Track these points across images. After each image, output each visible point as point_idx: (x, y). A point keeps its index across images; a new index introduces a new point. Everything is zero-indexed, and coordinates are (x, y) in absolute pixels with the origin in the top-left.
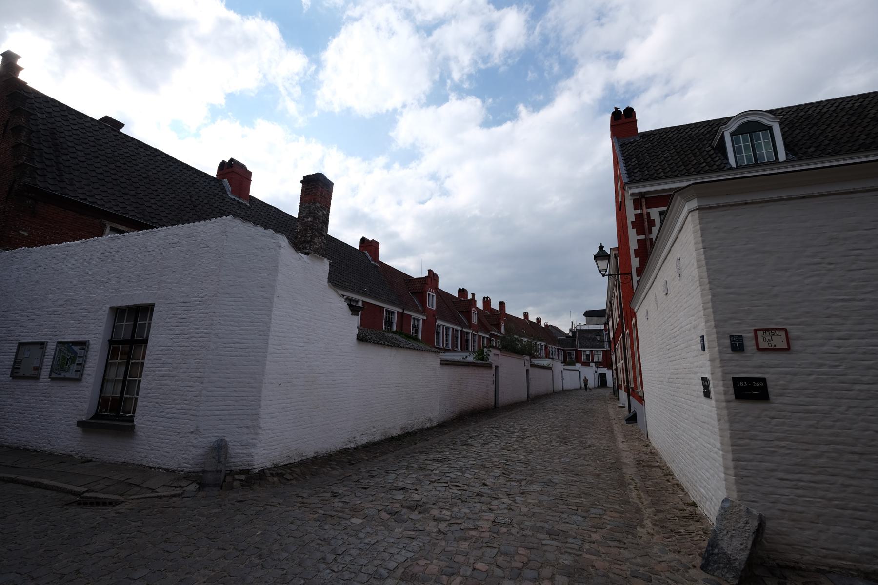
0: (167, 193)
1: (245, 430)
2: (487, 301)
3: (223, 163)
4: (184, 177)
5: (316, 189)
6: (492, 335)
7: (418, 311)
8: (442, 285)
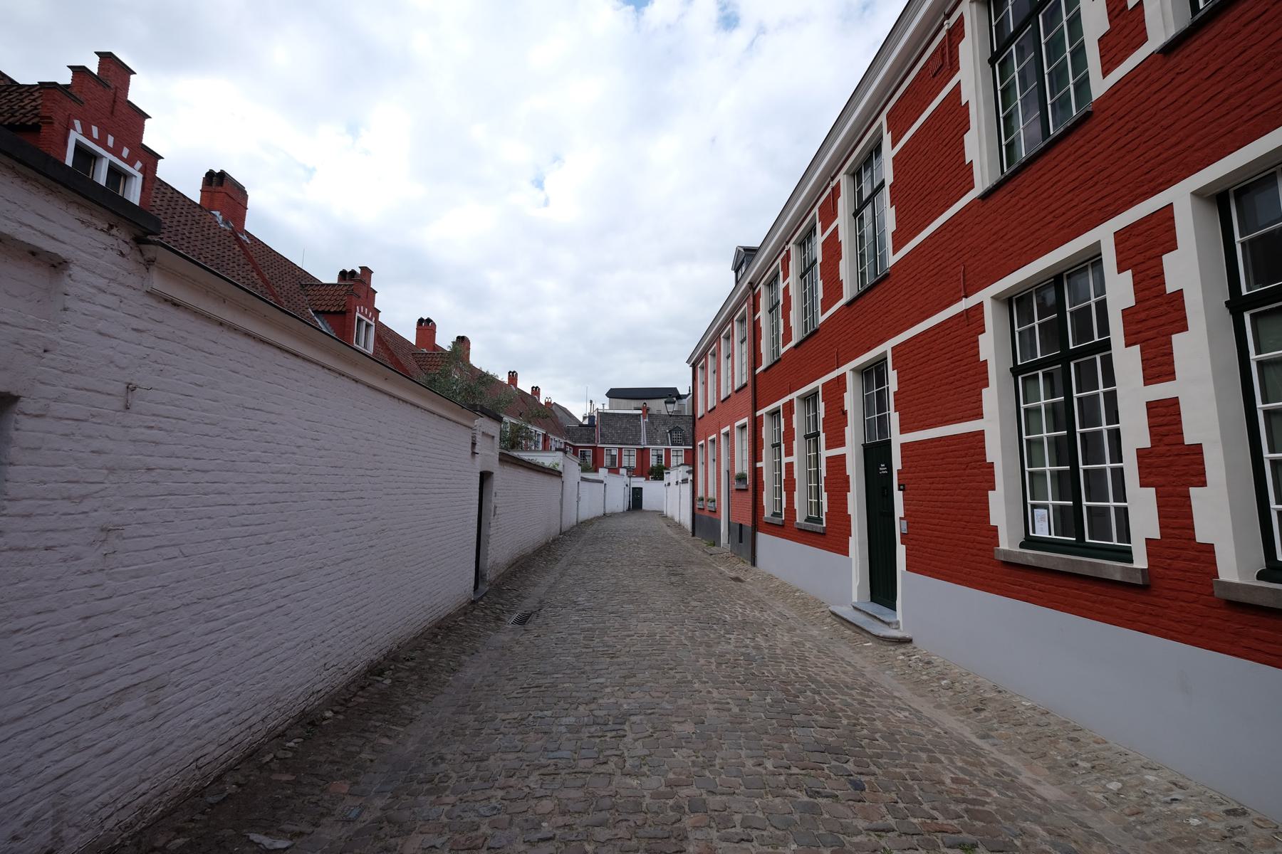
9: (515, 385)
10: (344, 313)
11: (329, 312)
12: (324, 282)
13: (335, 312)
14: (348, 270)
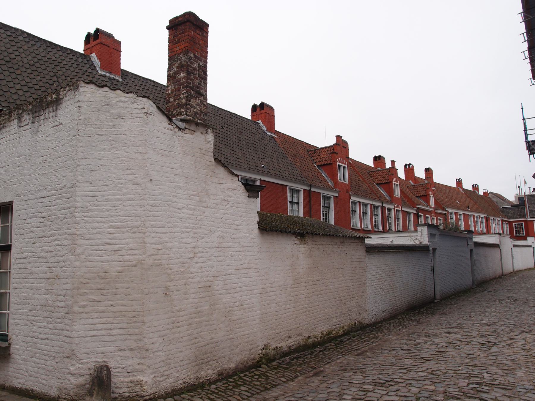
0: (32, 76)
1: (128, 353)
2: (409, 169)
3: (89, 36)
4: (48, 56)
5: (188, 35)
6: (419, 210)
7: (328, 188)
8: (354, 154)
9: (461, 187)
10: (389, 183)
11: (382, 183)
12: (320, 146)
13: (385, 183)
14: (377, 156)
